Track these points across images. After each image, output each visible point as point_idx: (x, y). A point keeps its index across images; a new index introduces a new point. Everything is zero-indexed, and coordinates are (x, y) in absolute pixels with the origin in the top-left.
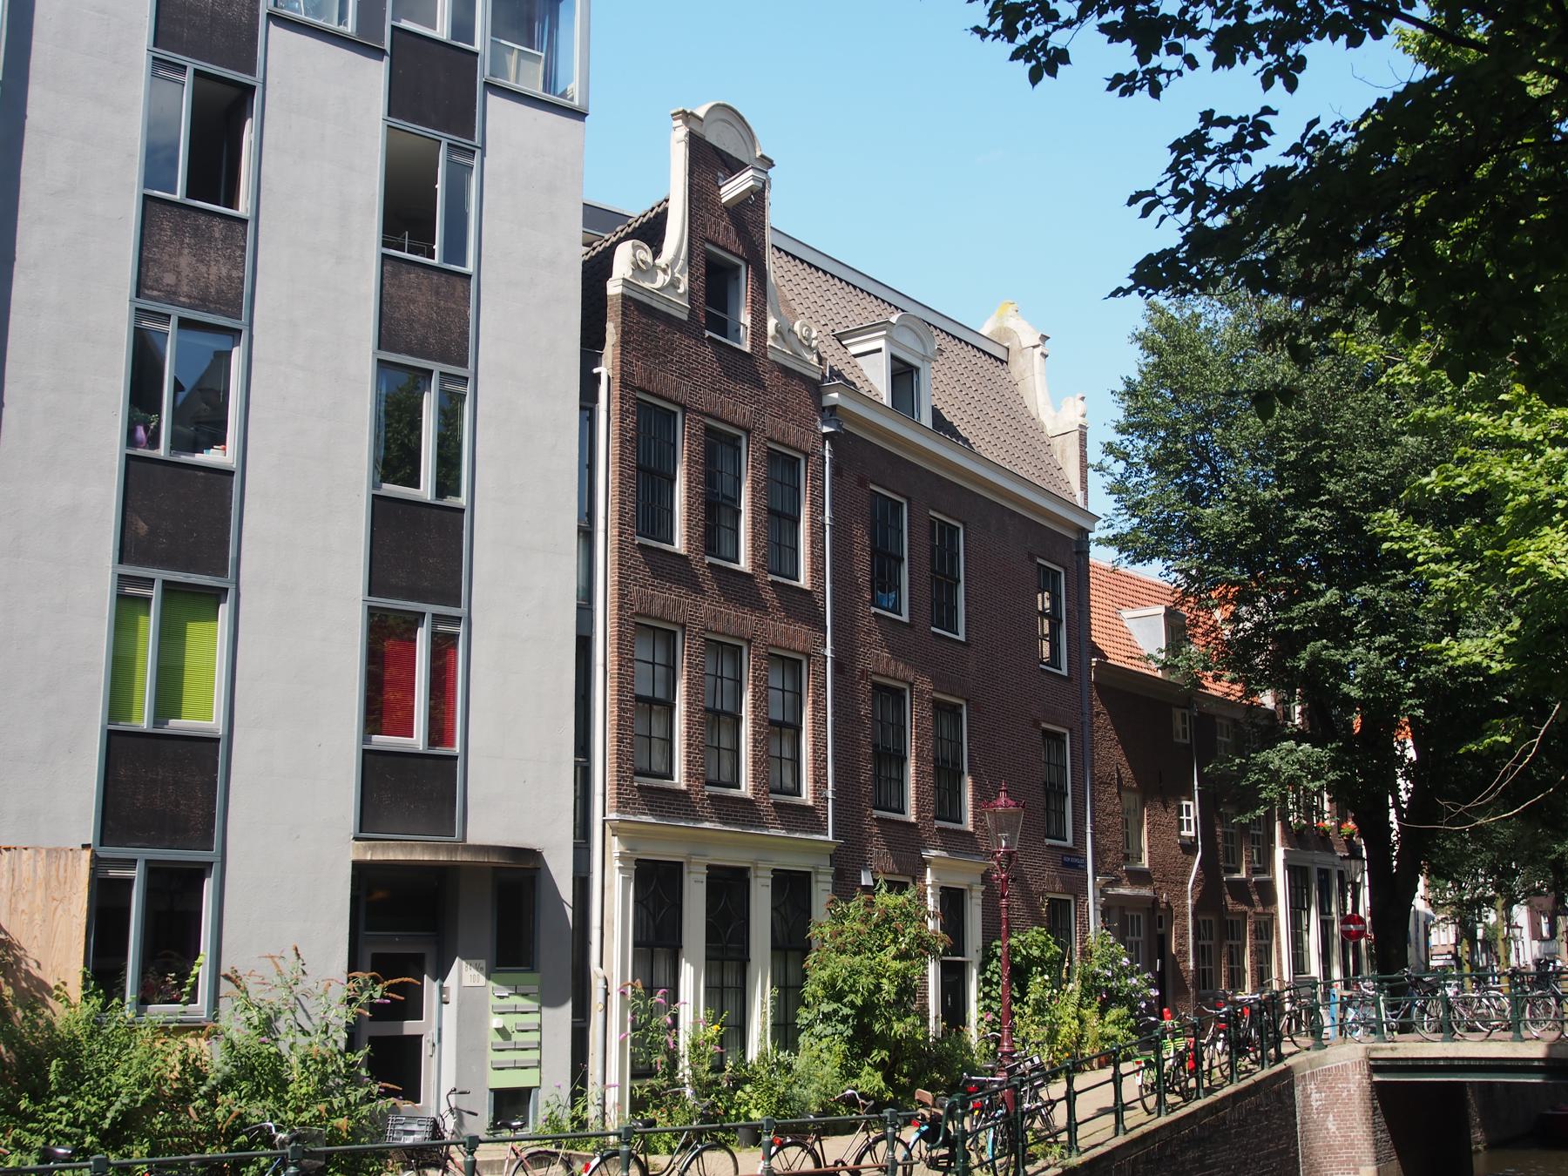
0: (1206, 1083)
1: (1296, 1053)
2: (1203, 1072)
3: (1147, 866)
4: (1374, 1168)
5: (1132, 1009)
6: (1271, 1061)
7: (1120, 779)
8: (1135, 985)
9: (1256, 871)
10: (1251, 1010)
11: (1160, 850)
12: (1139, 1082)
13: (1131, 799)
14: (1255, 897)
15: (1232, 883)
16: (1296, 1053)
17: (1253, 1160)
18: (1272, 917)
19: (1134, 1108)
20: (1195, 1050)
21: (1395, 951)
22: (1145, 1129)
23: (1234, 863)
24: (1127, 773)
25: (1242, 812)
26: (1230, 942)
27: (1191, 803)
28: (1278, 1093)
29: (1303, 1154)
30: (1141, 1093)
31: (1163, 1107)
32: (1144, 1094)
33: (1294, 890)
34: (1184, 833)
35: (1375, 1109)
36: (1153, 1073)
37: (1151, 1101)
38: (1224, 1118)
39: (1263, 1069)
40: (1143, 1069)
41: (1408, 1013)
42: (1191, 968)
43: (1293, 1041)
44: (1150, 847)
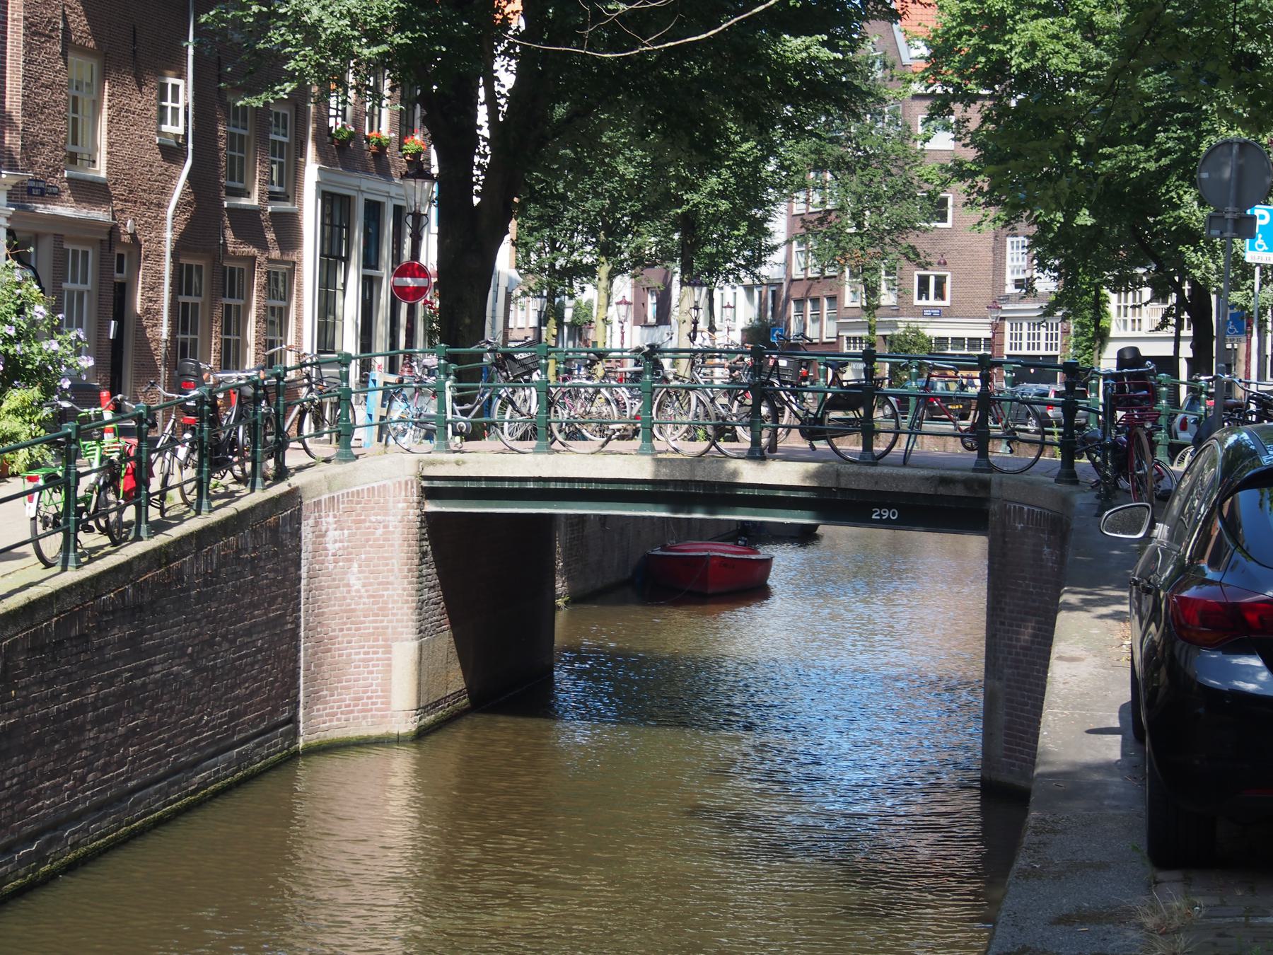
0: (154, 514)
1: (308, 466)
2: (149, 495)
3: (103, 174)
4: (415, 644)
5: (49, 390)
6: (266, 479)
7: (67, 31)
8: (55, 353)
9: (274, 197)
10: (240, 396)
11: (126, 151)
12: (31, 510)
13: (84, 68)
14: (270, 236)
15: (236, 212)
16: (308, 466)
17: (224, 637)
18: (292, 269)
19: (23, 556)
20: (138, 459)
21: (467, 321)
22: (34, 593)
23: (241, 181)
24: (80, 23)
25: (253, 92)
26: (227, 301)
27: (180, 82)
28: (275, 530)
29: (307, 623)
30: (34, 530)
31: (72, 555)
32: (40, 531)
33: (327, 229)
34: (167, 128)
35: (424, 554)
36: (59, 497)
37: (52, 545)
38: (180, 571)
39: (253, 490)
40: (40, 489)
41: (486, 409)
42: (165, 337)
43: (305, 448)
44: (111, 145)
